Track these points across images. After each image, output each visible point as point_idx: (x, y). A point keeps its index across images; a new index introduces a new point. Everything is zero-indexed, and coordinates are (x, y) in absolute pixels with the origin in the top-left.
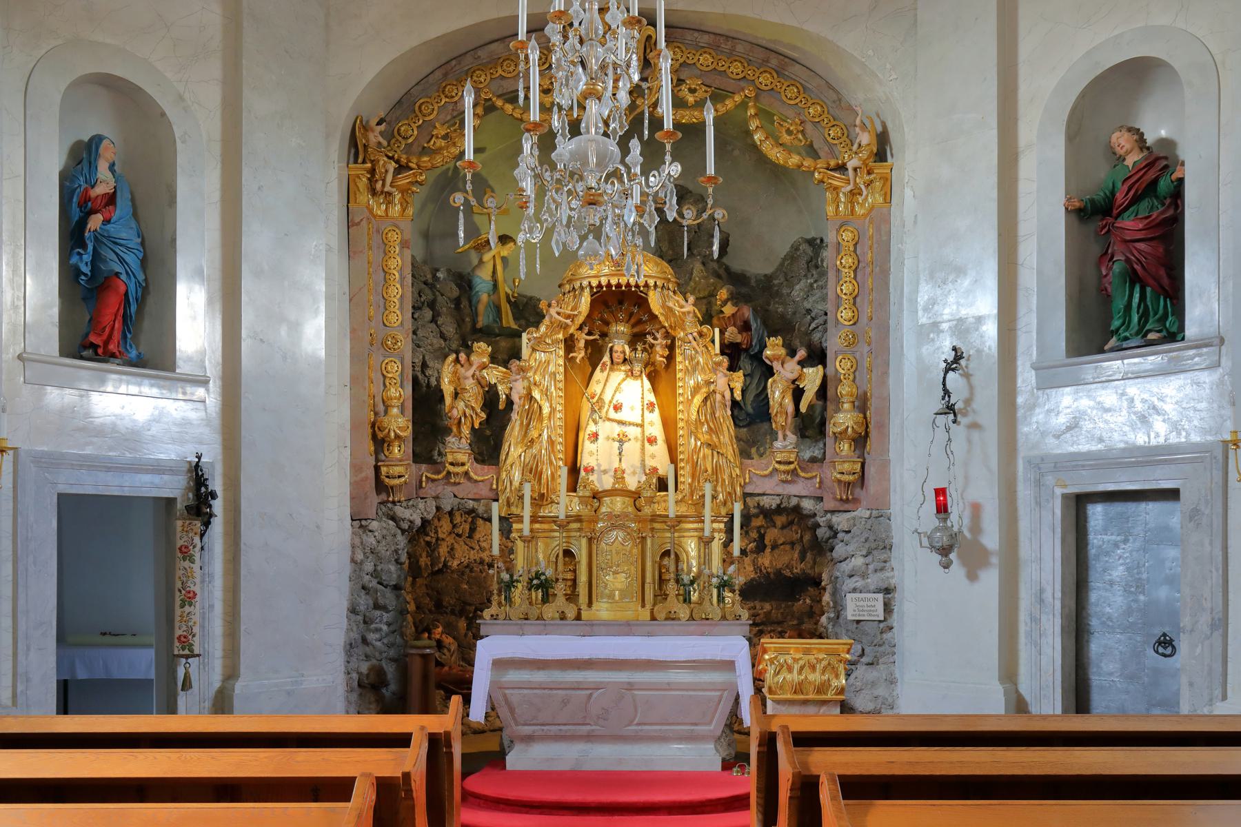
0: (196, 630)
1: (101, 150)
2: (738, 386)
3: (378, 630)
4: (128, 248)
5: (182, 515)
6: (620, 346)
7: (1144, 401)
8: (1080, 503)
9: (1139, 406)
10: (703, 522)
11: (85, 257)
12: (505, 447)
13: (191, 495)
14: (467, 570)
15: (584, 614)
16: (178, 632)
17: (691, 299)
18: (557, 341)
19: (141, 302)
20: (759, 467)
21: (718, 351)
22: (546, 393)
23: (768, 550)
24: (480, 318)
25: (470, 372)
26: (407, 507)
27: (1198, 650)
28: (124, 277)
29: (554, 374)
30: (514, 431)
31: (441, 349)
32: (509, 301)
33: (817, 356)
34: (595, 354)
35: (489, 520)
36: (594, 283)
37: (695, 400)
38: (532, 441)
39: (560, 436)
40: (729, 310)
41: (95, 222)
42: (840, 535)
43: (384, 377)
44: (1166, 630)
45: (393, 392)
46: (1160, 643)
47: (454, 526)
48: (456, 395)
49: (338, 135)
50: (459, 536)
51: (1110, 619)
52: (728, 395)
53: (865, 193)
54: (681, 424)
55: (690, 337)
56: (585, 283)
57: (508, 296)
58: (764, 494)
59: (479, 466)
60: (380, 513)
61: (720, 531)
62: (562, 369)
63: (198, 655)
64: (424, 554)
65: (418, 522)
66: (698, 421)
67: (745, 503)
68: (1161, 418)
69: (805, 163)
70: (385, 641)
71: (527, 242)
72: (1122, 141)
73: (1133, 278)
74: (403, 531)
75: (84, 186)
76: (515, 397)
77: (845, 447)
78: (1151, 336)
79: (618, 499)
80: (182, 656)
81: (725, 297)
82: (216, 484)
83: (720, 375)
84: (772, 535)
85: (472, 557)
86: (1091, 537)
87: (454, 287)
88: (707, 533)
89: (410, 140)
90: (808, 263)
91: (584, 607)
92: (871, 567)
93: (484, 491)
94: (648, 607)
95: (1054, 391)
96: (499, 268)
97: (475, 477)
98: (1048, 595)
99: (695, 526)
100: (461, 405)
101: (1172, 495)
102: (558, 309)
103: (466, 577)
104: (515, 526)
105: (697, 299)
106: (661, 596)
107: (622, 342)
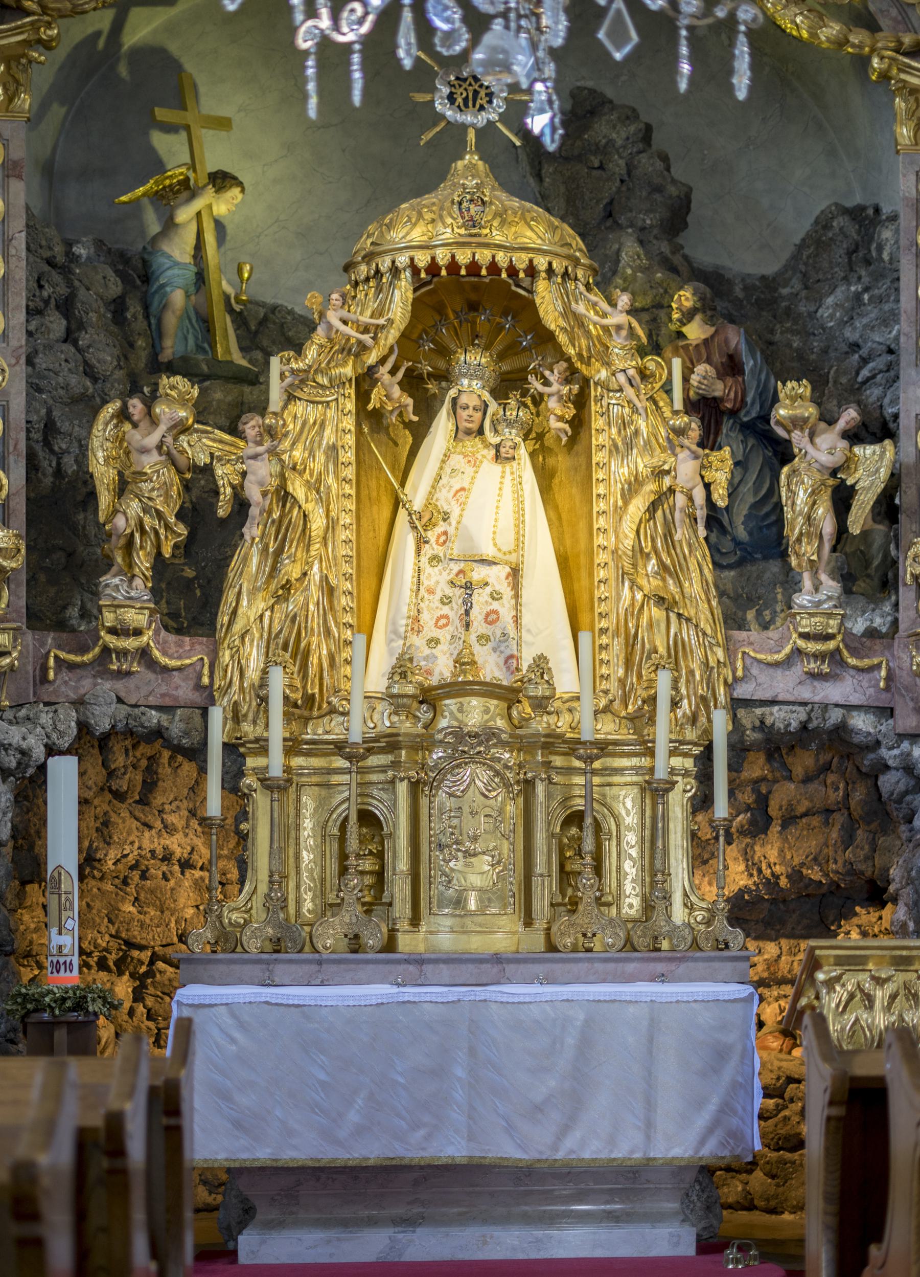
2: (721, 477)
6: (471, 389)
12: (230, 597)
14: (136, 875)
15: (406, 942)
18: (338, 383)
20: (760, 645)
21: (678, 405)
22: (316, 486)
23: (775, 828)
24: (168, 343)
25: (153, 439)
26: (15, 722)
30: (249, 562)
32: (230, 310)
34: (425, 390)
35: (196, 753)
36: (422, 259)
37: (632, 508)
38: (287, 587)
39: (348, 577)
40: (695, 332)
47: (111, 774)
48: (122, 488)
50: (119, 796)
52: (699, 495)
54: (602, 557)
55: (622, 378)
56: (402, 260)
57: (227, 298)
58: (773, 702)
59: (172, 638)
61: (686, 774)
66: (639, 553)
67: (735, 719)
69: (854, 39)
71: (325, 43)
76: (253, 493)
79: (475, 701)
81: (688, 304)
84: (783, 795)
85: (147, 845)
87: (110, 274)
88: (661, 773)
90: (850, 253)
91: (403, 925)
93: (184, 691)
94: (540, 924)
96: (210, 238)
97: (164, 660)
99: (634, 761)
100: (134, 507)
102: (344, 313)
103: (131, 889)
104: (251, 762)
107: (476, 384)
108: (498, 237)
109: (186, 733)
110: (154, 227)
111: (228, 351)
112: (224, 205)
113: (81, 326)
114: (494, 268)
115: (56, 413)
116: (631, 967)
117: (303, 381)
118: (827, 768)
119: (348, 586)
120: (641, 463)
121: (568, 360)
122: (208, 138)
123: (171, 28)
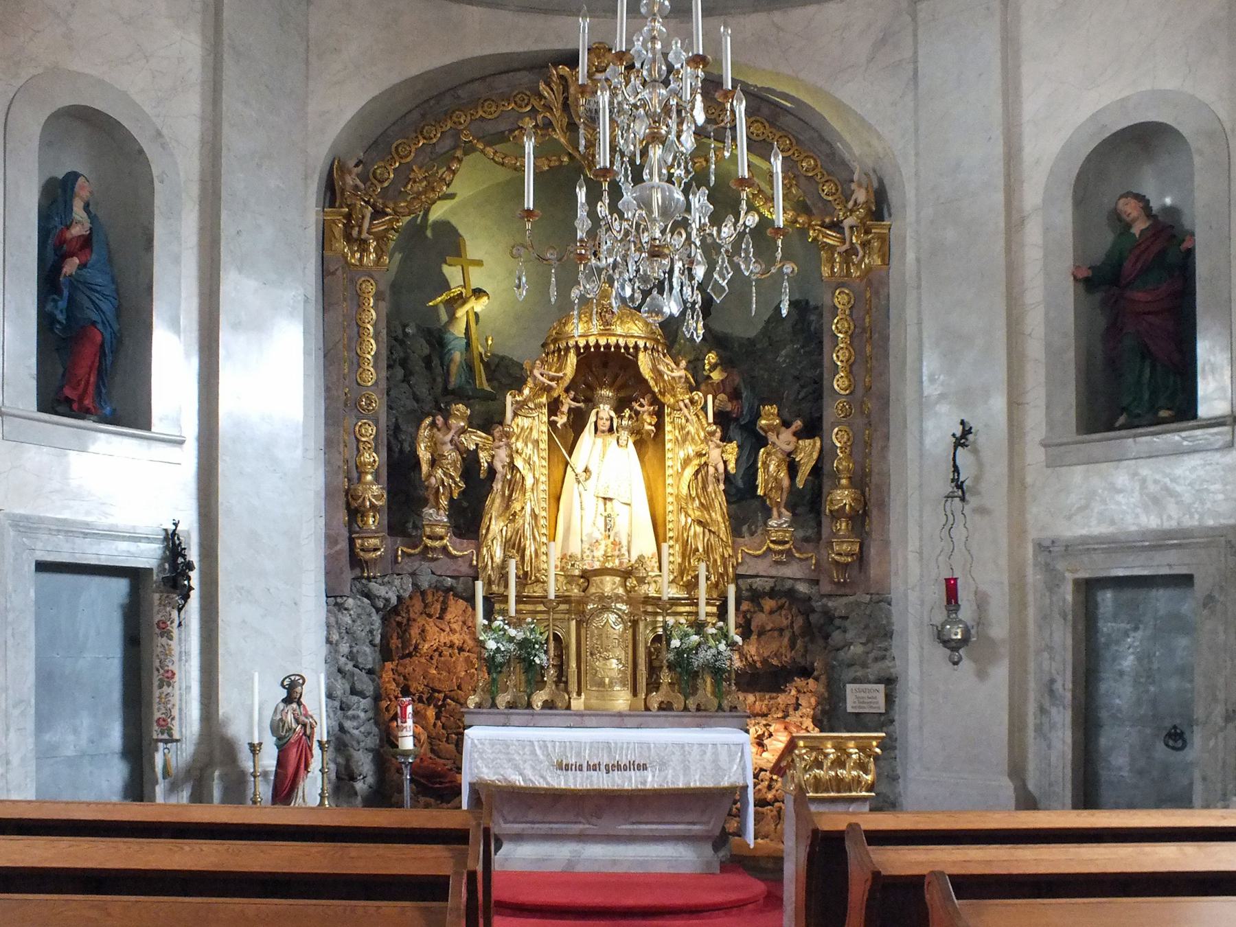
0: (175, 712)
1: (77, 189)
2: (732, 459)
3: (354, 717)
4: (103, 295)
5: (158, 587)
6: (606, 411)
7: (1156, 482)
8: (1089, 588)
9: (1152, 488)
10: (697, 605)
11: (60, 303)
12: (486, 520)
13: (167, 566)
16: (157, 715)
17: (683, 364)
19: (115, 352)
20: (749, 546)
21: (711, 420)
22: (528, 461)
23: (754, 637)
25: (449, 437)
26: (383, 584)
27: (1212, 743)
28: (100, 326)
29: (537, 441)
30: (494, 504)
31: (414, 411)
32: (482, 360)
33: (812, 429)
34: (578, 422)
36: (582, 343)
38: (514, 515)
39: (544, 509)
41: (71, 266)
42: (837, 622)
43: (358, 441)
44: (1177, 722)
45: (367, 457)
46: (1169, 735)
47: (426, 606)
48: (433, 463)
49: (316, 177)
51: (1119, 710)
52: (721, 467)
53: (861, 253)
54: (670, 499)
55: (681, 404)
56: (571, 343)
60: (355, 590)
62: (545, 437)
63: (177, 741)
64: (395, 636)
65: (394, 601)
67: (737, 586)
68: (1173, 500)
70: (362, 729)
72: (1131, 209)
73: (1145, 353)
74: (378, 610)
75: (60, 227)
76: (498, 466)
77: (843, 526)
78: (1163, 414)
79: (608, 578)
80: (161, 741)
82: (193, 555)
83: (712, 445)
84: (759, 619)
85: (443, 641)
86: (1100, 624)
89: (386, 184)
92: (871, 656)
93: (464, 569)
95: (1064, 469)
96: (472, 324)
97: (454, 552)
98: (1058, 686)
99: (687, 609)
101: (1186, 581)
103: (434, 661)
104: (497, 606)
105: (689, 362)
106: (653, 685)
107: (607, 407)
108: (619, 331)
109: (465, 590)
110: (444, 317)
111: (481, 383)
112: (479, 306)
113: (411, 374)
114: (617, 346)
115: (400, 421)
116: (686, 720)
117: (522, 407)
118: (781, 607)
119: (544, 514)
120: (690, 449)
121: (653, 393)
122: (473, 272)
123: (453, 211)
